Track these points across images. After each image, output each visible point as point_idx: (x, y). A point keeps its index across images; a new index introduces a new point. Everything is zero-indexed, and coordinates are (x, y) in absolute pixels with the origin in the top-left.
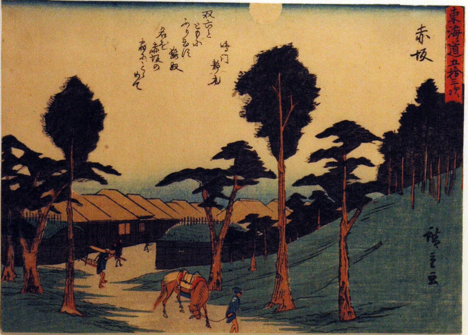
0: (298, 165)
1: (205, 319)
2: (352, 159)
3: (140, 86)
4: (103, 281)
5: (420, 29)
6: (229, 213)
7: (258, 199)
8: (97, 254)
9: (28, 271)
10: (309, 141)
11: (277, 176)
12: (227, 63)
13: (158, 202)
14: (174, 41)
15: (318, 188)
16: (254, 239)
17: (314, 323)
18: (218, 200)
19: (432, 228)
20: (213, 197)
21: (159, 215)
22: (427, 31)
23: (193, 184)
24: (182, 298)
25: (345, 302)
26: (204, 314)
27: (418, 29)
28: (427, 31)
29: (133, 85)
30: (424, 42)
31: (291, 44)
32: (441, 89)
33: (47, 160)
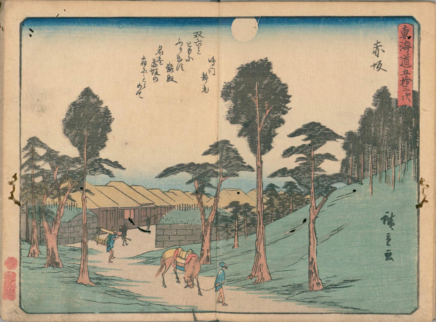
0: (273, 160)
1: (198, 289)
2: (320, 155)
3: (141, 95)
4: (112, 257)
5: (376, 44)
6: (216, 201)
7: (240, 189)
8: (108, 234)
9: (51, 250)
10: (282, 140)
11: (256, 169)
12: (214, 75)
14: (170, 57)
15: (290, 179)
16: (237, 221)
17: (287, 292)
18: (207, 190)
19: (387, 212)
20: (203, 187)
22: (381, 46)
23: (186, 176)
25: (314, 275)
26: (197, 285)
27: (375, 45)
28: (381, 46)
29: (137, 94)
30: (379, 56)
31: (266, 58)
32: (394, 94)
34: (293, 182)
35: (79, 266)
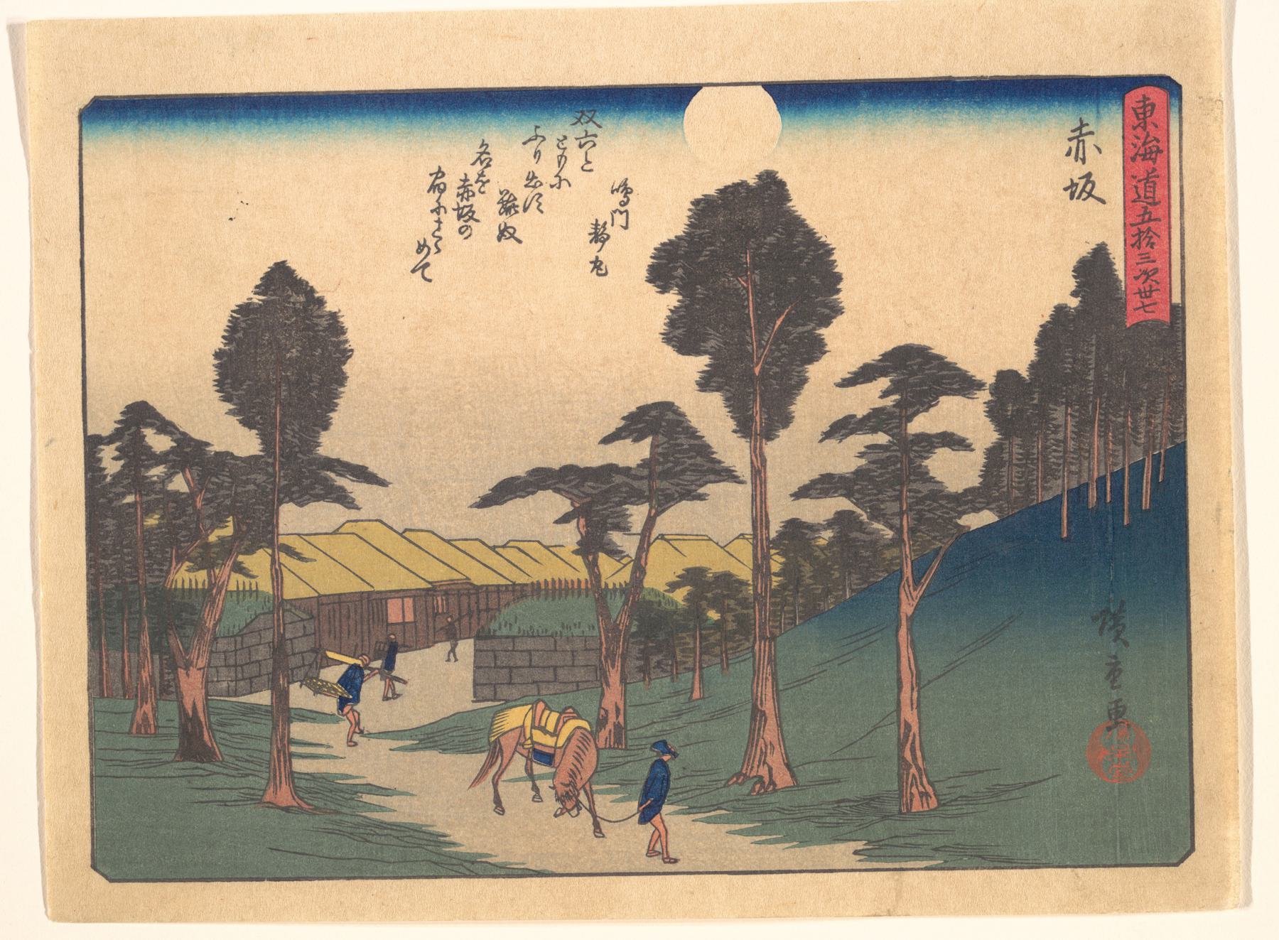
7: (709, 533)
8: (344, 668)
10: (823, 394)
13: (474, 548)
15: (844, 504)
16: (659, 634)
21: (481, 577)
23: (553, 503)
24: (539, 769)
29: (413, 271)
33: (224, 458)
34: (854, 512)
35: (267, 757)
